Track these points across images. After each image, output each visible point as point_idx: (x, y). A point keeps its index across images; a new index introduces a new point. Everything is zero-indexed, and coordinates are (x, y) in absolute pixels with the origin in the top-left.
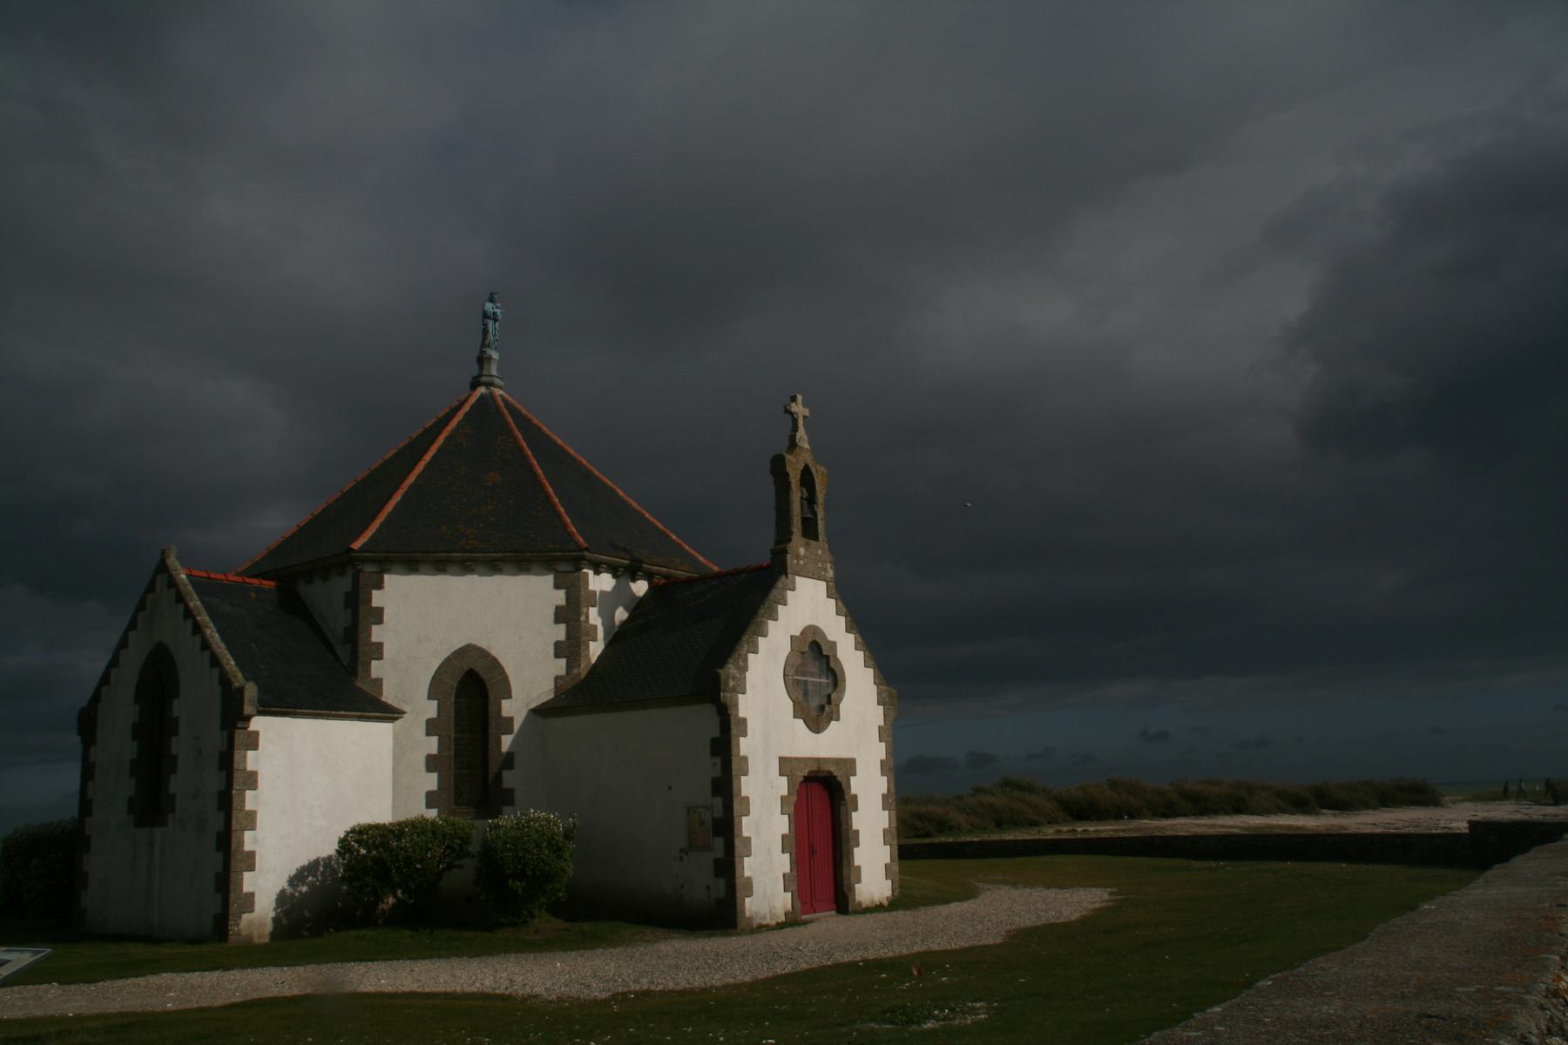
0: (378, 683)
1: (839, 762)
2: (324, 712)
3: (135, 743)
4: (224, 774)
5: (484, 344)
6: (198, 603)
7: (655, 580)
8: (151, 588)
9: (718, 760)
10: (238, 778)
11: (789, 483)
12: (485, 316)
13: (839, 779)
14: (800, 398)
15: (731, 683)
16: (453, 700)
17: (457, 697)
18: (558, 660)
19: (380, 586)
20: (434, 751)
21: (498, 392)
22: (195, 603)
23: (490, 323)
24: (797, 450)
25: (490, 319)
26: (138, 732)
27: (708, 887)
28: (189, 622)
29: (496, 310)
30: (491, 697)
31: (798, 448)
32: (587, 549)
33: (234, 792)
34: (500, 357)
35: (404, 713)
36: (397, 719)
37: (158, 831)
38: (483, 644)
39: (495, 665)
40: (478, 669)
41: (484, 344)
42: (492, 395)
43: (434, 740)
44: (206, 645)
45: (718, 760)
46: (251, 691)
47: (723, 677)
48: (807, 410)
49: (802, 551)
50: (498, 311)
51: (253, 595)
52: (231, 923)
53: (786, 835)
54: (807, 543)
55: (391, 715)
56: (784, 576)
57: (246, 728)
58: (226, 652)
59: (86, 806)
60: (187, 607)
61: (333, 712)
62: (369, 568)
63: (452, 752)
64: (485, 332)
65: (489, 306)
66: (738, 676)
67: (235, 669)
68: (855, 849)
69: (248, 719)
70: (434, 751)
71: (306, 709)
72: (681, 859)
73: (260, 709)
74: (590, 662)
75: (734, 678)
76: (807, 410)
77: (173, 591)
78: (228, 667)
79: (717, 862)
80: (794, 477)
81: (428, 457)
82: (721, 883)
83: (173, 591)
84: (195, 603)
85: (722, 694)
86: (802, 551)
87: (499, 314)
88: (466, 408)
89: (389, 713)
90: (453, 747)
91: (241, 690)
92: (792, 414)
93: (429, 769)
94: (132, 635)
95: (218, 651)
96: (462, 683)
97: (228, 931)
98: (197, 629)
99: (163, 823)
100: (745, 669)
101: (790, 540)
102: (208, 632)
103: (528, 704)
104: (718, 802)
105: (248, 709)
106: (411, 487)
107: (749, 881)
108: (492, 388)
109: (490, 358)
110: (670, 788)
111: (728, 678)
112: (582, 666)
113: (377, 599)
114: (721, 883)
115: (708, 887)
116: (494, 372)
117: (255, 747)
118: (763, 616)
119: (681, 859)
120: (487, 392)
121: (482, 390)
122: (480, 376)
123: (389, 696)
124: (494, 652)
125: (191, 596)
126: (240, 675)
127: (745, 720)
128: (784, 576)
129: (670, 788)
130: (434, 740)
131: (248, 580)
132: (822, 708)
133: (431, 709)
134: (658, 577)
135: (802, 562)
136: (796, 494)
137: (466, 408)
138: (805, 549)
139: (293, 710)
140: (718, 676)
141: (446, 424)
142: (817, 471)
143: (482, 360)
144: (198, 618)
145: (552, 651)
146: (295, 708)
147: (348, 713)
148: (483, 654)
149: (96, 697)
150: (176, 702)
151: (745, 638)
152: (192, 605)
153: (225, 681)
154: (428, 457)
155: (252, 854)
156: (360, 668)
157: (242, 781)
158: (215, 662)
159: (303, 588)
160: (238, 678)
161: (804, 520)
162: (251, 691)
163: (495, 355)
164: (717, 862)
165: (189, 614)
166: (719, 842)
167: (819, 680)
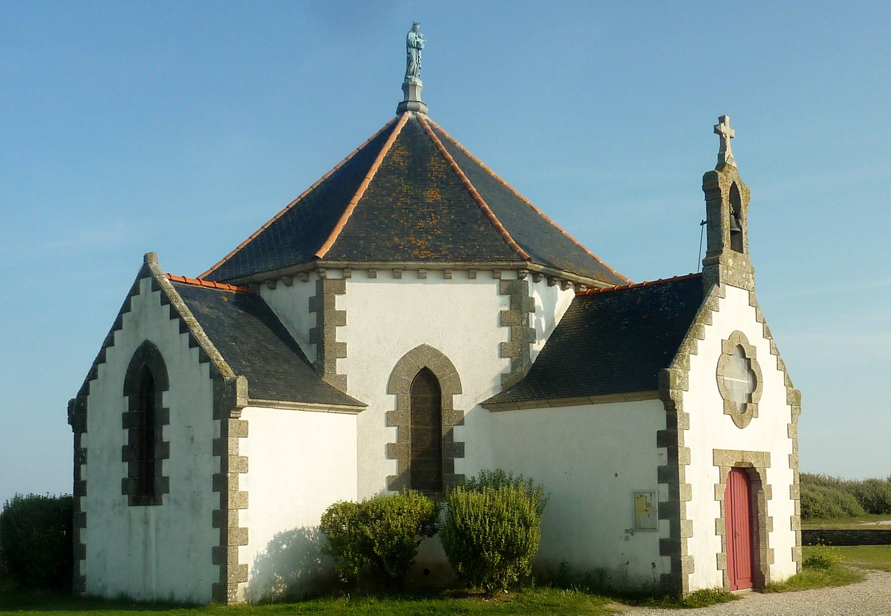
0: (343, 379)
1: (757, 454)
2: (302, 404)
3: (126, 432)
4: (218, 458)
5: (409, 73)
6: (183, 304)
7: (581, 290)
8: (135, 291)
9: (664, 450)
10: (232, 463)
11: (721, 199)
12: (409, 45)
13: (758, 470)
14: (727, 118)
15: (678, 381)
16: (409, 395)
17: (413, 392)
18: (503, 359)
19: (342, 291)
20: (394, 441)
21: (424, 117)
22: (180, 304)
23: (414, 51)
24: (726, 168)
25: (414, 47)
26: (127, 420)
27: (654, 565)
28: (176, 322)
29: (418, 40)
30: (443, 393)
31: (727, 166)
32: (529, 260)
33: (229, 475)
34: (423, 84)
35: (367, 406)
36: (360, 411)
37: (152, 510)
38: (435, 345)
39: (447, 363)
40: (431, 368)
41: (409, 73)
42: (418, 119)
43: (393, 430)
44: (194, 343)
45: (664, 450)
46: (242, 384)
47: (671, 375)
48: (734, 131)
49: (731, 262)
50: (421, 41)
51: (226, 299)
52: (229, 591)
53: (217, 511)
54: (735, 254)
55: (355, 408)
56: (716, 286)
57: (238, 418)
58: (214, 349)
59: (80, 486)
60: (173, 308)
61: (309, 404)
62: (331, 275)
63: (409, 442)
64: (409, 60)
65: (412, 35)
66: (682, 375)
67: (225, 364)
68: (770, 534)
69: (240, 409)
70: (394, 441)
71: (287, 401)
72: (627, 539)
73: (250, 400)
74: (530, 361)
75: (680, 377)
76: (734, 131)
77: (158, 293)
78: (218, 363)
79: (662, 542)
80: (725, 194)
81: (371, 175)
82: (667, 560)
83: (158, 293)
84: (180, 304)
85: (671, 391)
86: (731, 262)
87: (421, 43)
88: (398, 131)
89: (354, 406)
90: (410, 437)
91: (233, 383)
92: (720, 133)
93: (390, 456)
94: (117, 334)
95: (207, 348)
96: (416, 380)
97: (227, 598)
98: (184, 327)
99: (157, 502)
100: (687, 369)
101: (721, 252)
102: (196, 331)
103: (476, 399)
104: (664, 489)
105: (240, 401)
106: (360, 202)
107: (691, 560)
108: (418, 113)
109: (415, 85)
110: (616, 475)
111: (676, 377)
112: (524, 365)
113: (340, 303)
114: (667, 560)
115: (654, 565)
116: (418, 99)
117: (246, 435)
118: (701, 322)
119: (627, 539)
120: (414, 117)
121: (409, 115)
122: (407, 102)
123: (352, 391)
124: (445, 353)
125: (176, 299)
126: (229, 370)
127: (688, 415)
128: (716, 286)
129: (616, 475)
130: (393, 430)
131: (218, 285)
132: (745, 406)
133: (390, 403)
134: (584, 286)
135: (730, 272)
136: (726, 210)
137: (398, 131)
138: (733, 260)
139: (277, 402)
140: (668, 374)
141: (385, 141)
142: (742, 189)
143: (407, 87)
144: (185, 318)
145: (496, 351)
146: (279, 400)
147: (321, 405)
148: (437, 354)
149: (85, 391)
150: (165, 394)
151: (687, 341)
152: (178, 306)
153: (216, 375)
154: (371, 175)
155: (245, 531)
156: (326, 365)
157: (235, 465)
158: (205, 358)
159: (266, 294)
160: (229, 373)
161: (733, 233)
162: (242, 384)
163: (419, 83)
164: (662, 542)
165: (175, 314)
166: (664, 526)
167: (742, 381)
